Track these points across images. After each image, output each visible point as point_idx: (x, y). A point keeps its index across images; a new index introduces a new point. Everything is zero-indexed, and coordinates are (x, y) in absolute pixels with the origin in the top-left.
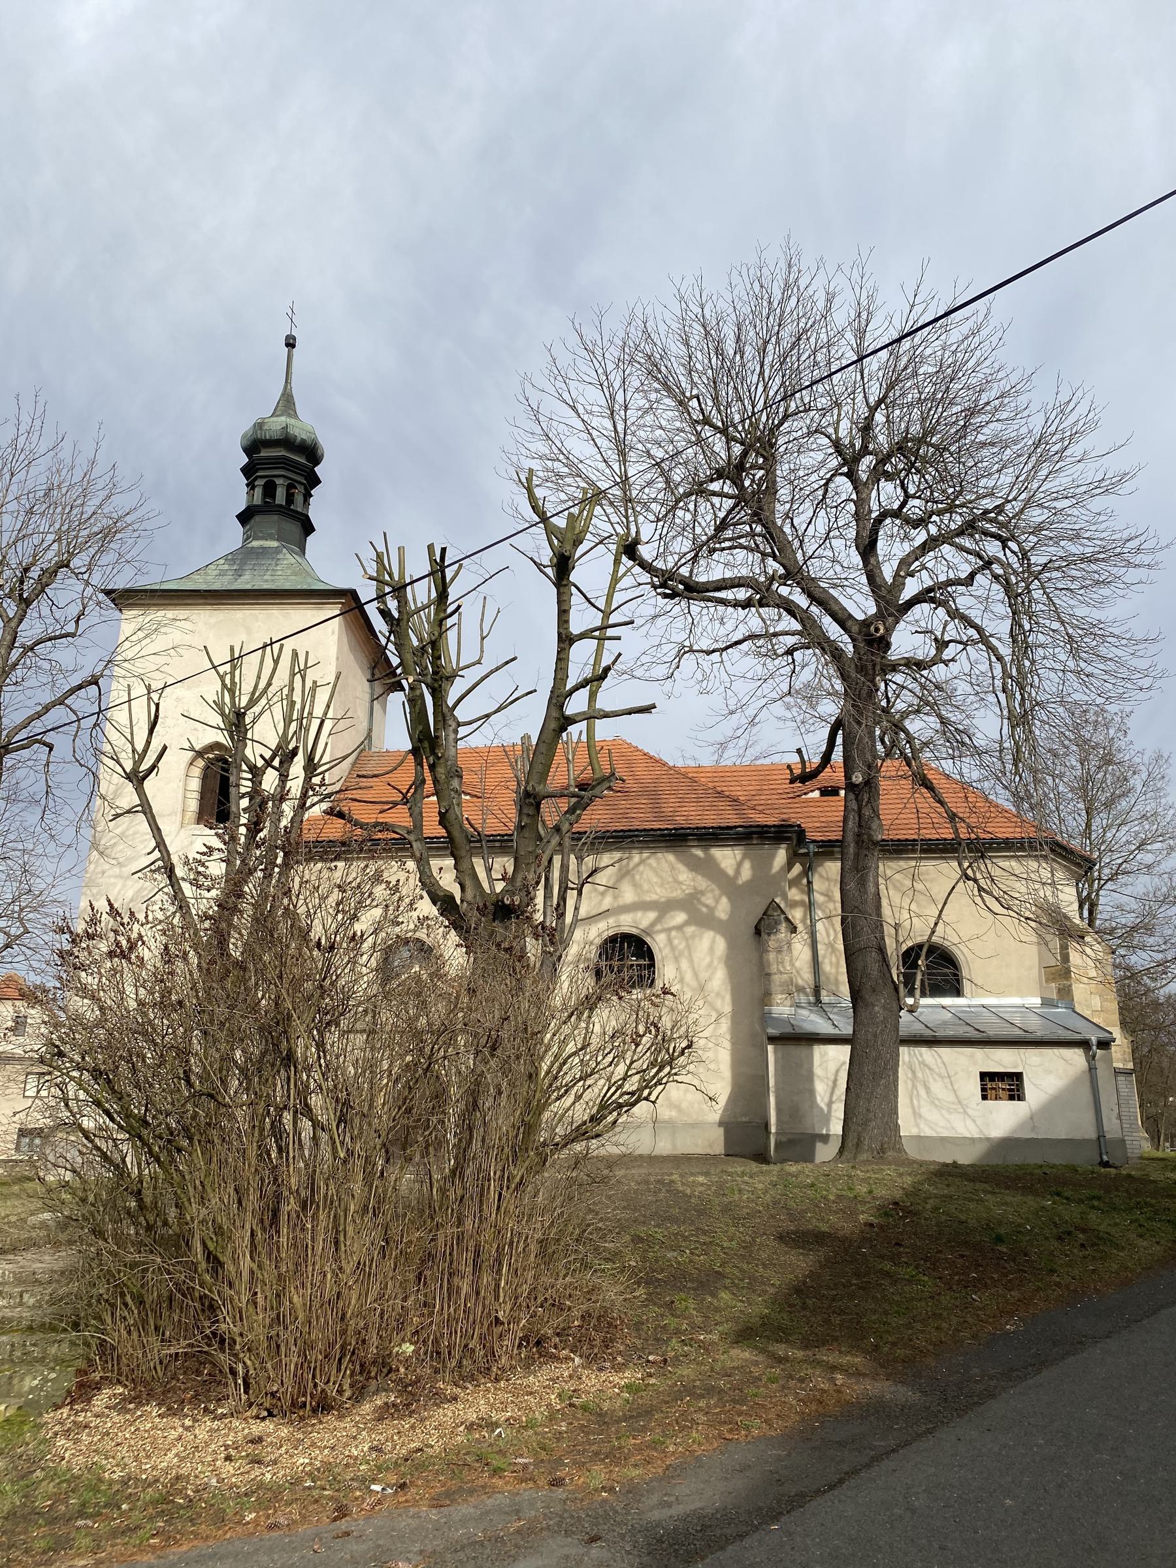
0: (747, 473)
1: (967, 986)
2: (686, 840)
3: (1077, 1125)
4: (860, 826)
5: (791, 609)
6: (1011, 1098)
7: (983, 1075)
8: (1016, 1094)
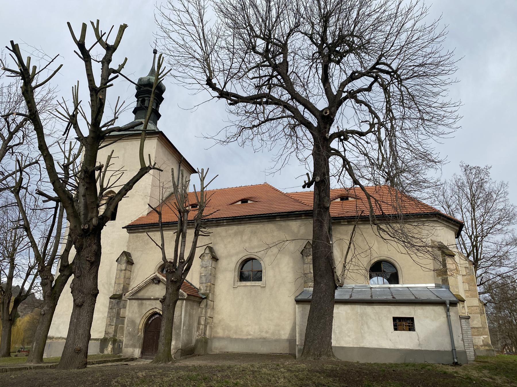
0: (275, 57)
1: (400, 280)
2: (275, 218)
3: (442, 344)
4: (320, 201)
5: (277, 102)
6: (410, 330)
7: (395, 319)
8: (411, 328)
